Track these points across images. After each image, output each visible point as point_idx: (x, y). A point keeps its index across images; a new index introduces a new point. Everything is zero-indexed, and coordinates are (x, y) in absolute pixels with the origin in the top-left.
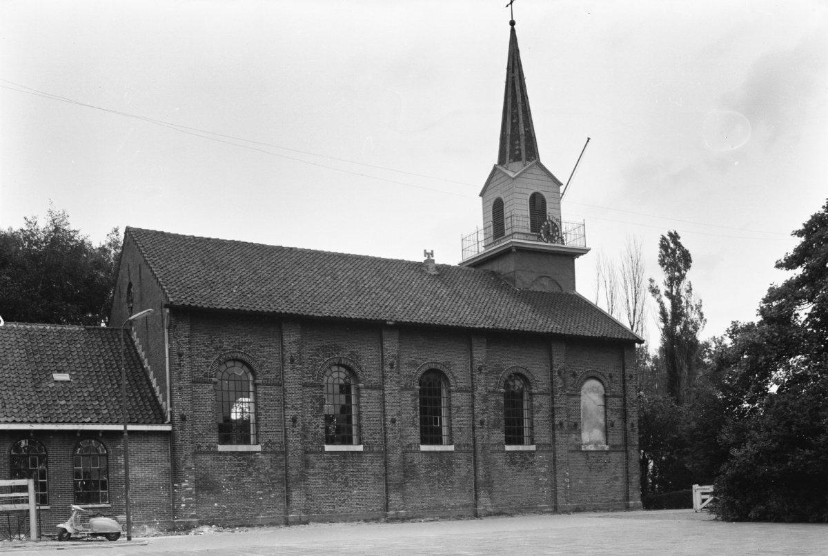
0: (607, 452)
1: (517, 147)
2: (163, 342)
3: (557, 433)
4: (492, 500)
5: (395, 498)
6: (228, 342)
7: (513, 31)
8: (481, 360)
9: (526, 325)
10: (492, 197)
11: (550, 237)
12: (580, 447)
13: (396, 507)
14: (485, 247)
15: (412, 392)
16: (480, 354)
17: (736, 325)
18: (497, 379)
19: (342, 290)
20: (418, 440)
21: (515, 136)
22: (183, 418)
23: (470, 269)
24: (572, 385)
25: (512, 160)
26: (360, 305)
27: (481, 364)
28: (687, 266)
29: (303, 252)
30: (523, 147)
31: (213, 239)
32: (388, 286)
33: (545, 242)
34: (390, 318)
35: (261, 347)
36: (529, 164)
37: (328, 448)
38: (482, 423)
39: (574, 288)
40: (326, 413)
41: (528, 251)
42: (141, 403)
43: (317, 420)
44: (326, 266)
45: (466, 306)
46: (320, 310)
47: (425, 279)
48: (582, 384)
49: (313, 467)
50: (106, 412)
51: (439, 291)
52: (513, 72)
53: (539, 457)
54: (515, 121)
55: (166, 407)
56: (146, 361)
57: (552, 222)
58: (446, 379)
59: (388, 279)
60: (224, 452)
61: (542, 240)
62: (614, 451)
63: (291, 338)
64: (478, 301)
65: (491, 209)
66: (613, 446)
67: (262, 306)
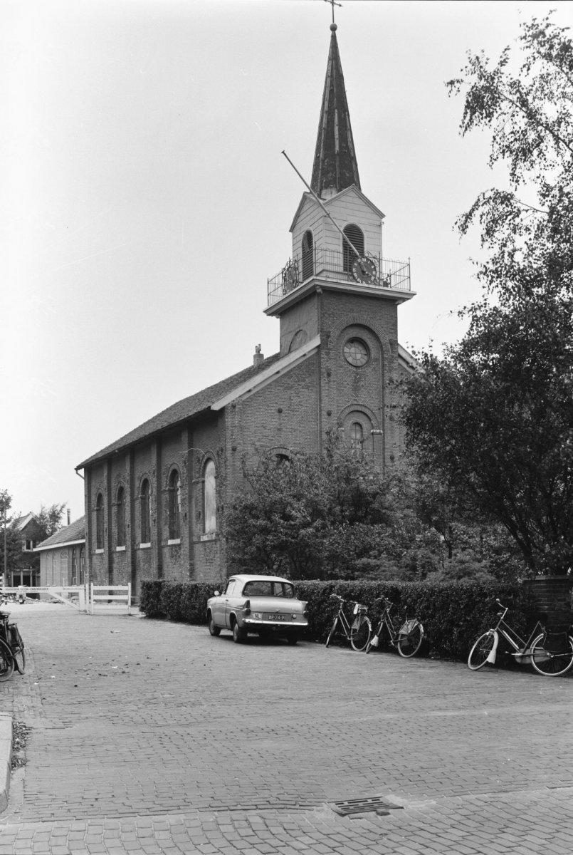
7: (334, 37)
10: (303, 227)
11: (364, 275)
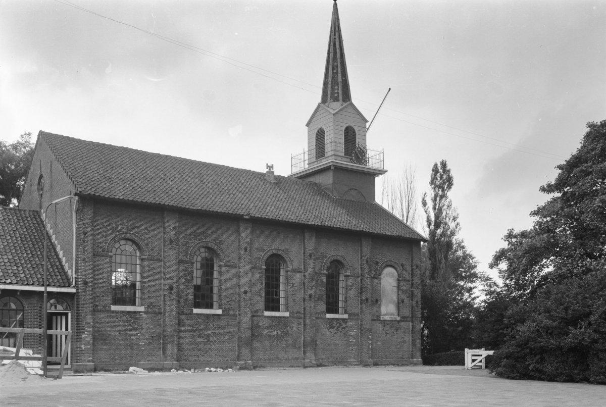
0: (399, 322)
1: (336, 91)
2: (71, 222)
3: (364, 306)
4: (316, 354)
5: (245, 351)
6: (122, 223)
8: (311, 248)
9: (345, 224)
12: (380, 317)
13: (245, 358)
14: (308, 164)
15: (259, 271)
16: (310, 243)
17: (511, 232)
18: (322, 263)
19: (208, 190)
20: (263, 307)
21: (335, 83)
22: (86, 283)
23: (299, 180)
24: (375, 271)
25: (332, 100)
26: (222, 203)
27: (311, 252)
28: (449, 187)
29: (176, 159)
30: (340, 92)
31: (107, 145)
32: (241, 189)
33: (355, 163)
34: (246, 214)
35: (147, 230)
36: (345, 104)
37: (196, 311)
38: (310, 296)
39: (374, 199)
40: (195, 283)
41: (351, 171)
42: (51, 270)
43: (188, 289)
44: (194, 171)
45: (300, 208)
46: (194, 205)
47: (267, 186)
48: (382, 271)
49: (183, 326)
50: (23, 275)
51: (279, 195)
52: (335, 35)
53: (350, 323)
54: (335, 71)
55: (72, 275)
56: (54, 237)
57: (361, 149)
58: (285, 261)
59: (241, 184)
60: (115, 311)
61: (353, 162)
62: (403, 321)
63: (171, 224)
64: (307, 204)
65: (315, 136)
66: (403, 317)
67: (149, 198)
